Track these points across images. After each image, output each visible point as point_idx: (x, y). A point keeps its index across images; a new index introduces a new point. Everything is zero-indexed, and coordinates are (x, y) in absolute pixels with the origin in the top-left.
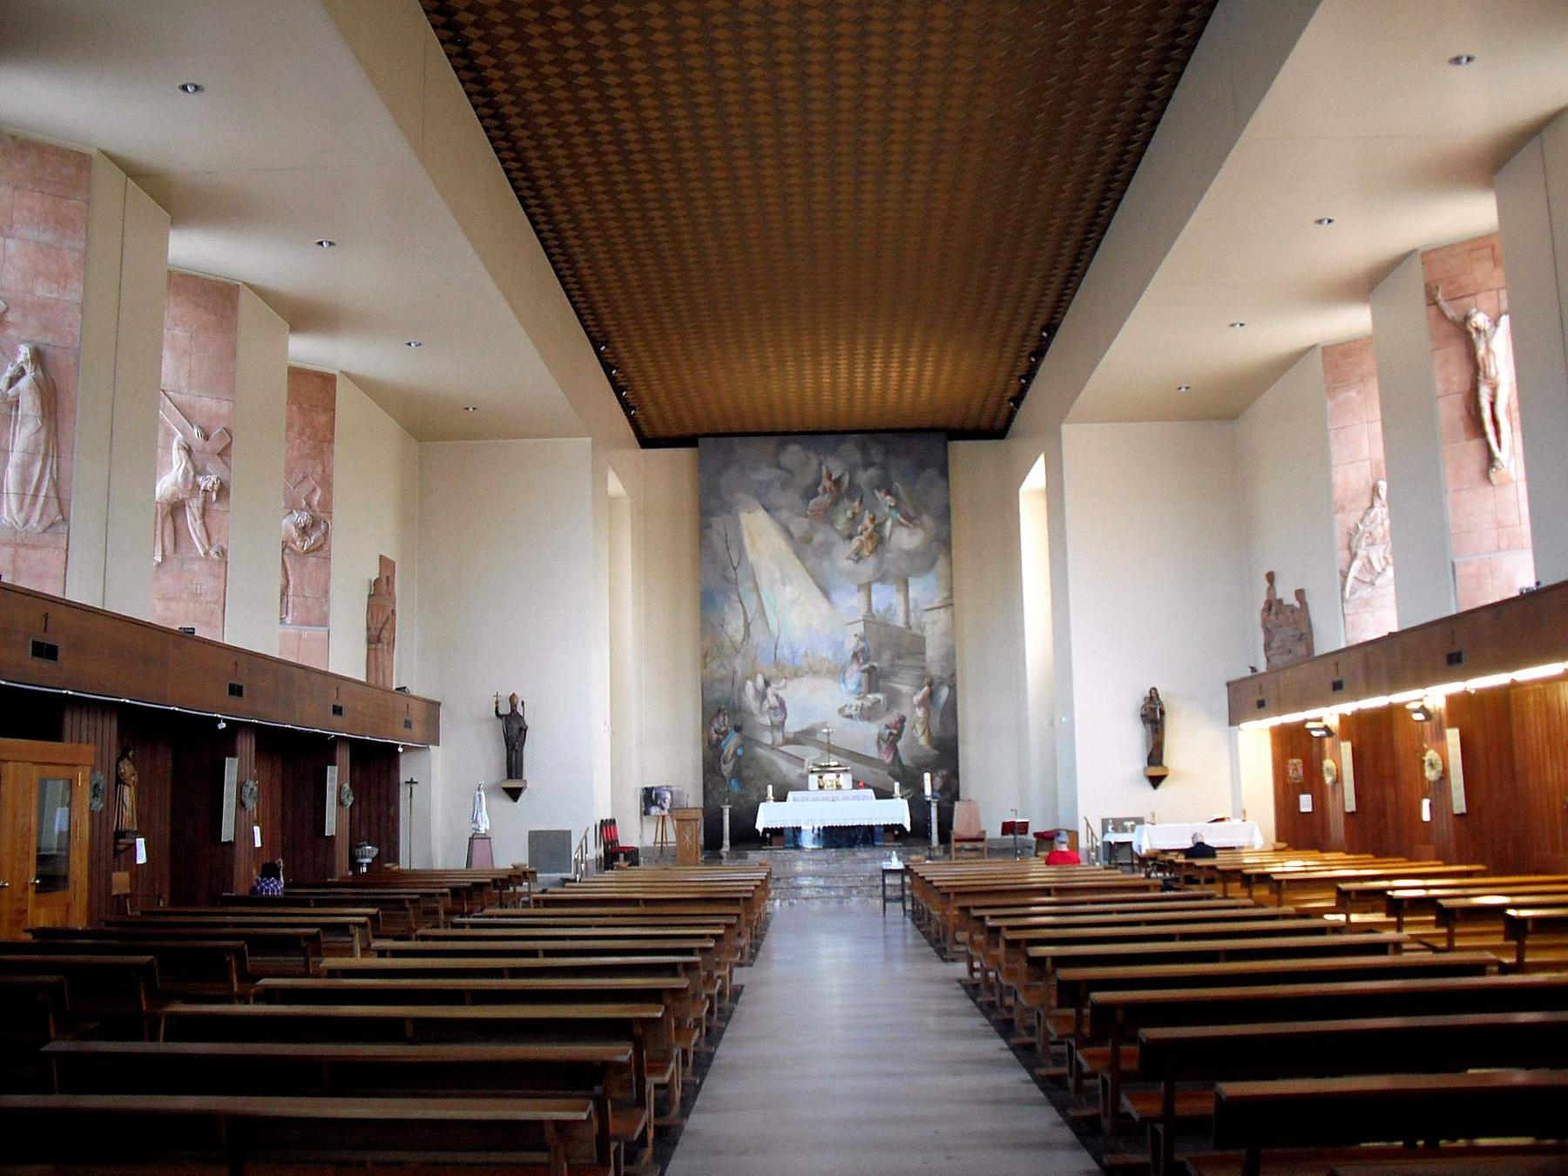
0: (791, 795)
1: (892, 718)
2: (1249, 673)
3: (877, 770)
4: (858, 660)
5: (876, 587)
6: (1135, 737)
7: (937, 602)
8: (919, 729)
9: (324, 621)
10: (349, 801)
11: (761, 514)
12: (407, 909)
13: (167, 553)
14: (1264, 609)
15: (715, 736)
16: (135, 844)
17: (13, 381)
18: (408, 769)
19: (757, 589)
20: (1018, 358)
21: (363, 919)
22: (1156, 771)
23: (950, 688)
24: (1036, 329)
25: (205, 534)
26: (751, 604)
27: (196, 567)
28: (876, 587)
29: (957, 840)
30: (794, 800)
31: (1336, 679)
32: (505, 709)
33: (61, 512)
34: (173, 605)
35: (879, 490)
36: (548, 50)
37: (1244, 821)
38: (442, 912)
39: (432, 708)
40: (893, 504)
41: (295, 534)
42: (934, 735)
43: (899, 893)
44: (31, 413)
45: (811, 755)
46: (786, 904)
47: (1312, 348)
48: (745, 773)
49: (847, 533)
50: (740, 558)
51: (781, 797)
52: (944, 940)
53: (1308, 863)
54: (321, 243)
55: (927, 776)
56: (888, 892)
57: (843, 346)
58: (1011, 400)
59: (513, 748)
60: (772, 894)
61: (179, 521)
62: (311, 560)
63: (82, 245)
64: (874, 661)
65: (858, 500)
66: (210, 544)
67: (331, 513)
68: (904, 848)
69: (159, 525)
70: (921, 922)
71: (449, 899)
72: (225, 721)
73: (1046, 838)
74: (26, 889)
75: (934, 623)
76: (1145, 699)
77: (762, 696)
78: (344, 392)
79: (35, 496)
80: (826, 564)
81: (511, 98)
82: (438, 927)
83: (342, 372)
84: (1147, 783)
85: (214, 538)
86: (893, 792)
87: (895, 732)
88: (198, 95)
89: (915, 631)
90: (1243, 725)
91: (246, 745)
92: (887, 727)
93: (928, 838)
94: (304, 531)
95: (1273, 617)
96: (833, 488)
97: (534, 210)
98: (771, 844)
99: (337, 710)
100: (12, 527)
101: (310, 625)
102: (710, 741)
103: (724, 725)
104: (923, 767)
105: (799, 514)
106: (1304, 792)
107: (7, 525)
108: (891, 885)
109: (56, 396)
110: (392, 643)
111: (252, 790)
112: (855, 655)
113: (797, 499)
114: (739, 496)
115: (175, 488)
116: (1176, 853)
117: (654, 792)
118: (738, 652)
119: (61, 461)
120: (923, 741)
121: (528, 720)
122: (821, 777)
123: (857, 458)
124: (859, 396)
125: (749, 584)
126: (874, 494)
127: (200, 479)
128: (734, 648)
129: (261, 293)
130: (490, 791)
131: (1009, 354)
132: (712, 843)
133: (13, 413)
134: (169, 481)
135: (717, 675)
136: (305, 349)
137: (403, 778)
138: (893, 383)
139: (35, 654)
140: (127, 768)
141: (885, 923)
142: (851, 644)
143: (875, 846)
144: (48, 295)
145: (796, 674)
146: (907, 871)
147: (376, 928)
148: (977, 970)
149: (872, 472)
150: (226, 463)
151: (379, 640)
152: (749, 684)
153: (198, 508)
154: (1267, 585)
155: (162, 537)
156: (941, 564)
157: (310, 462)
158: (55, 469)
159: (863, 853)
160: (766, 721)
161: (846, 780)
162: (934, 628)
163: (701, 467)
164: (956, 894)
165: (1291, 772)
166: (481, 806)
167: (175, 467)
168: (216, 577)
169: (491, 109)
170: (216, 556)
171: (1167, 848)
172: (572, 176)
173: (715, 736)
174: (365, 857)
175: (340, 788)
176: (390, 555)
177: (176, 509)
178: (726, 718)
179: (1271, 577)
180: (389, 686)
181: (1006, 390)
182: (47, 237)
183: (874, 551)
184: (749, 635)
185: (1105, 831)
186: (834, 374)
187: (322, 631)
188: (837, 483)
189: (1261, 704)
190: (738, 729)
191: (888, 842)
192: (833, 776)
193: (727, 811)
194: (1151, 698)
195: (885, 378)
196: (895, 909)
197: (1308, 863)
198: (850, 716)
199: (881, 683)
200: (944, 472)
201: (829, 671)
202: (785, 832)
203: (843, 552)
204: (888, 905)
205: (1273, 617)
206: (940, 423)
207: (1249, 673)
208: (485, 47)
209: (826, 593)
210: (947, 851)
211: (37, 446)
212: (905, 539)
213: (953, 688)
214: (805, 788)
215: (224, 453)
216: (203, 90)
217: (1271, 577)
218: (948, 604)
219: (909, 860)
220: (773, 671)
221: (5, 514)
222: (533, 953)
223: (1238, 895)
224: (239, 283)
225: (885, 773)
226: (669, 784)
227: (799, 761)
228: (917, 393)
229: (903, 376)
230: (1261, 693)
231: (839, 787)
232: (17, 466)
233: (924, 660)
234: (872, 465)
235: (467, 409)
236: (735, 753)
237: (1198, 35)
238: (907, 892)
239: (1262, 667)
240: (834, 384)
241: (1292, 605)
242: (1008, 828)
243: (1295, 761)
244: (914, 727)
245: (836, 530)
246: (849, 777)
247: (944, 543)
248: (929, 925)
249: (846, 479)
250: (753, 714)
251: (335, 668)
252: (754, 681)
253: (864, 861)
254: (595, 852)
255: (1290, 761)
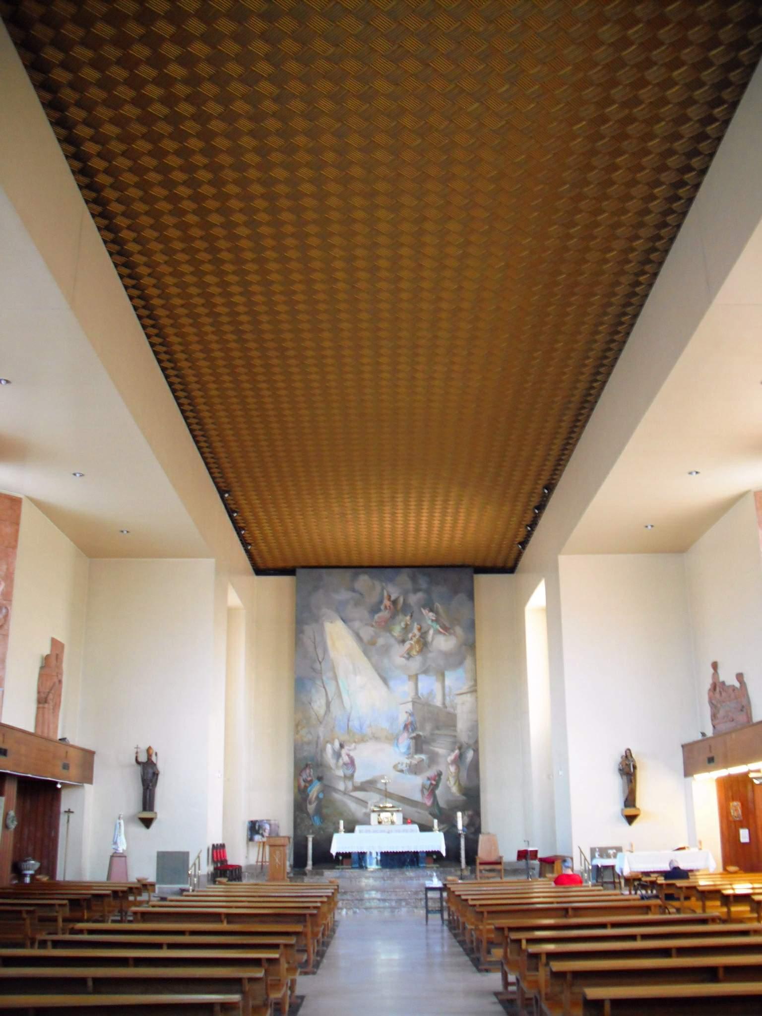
0: (358, 828)
1: (431, 773)
2: (700, 737)
3: (419, 810)
4: (408, 730)
5: (421, 677)
6: (615, 785)
7: (465, 688)
8: (452, 781)
11: (340, 624)
12: (24, 919)
14: (710, 690)
15: (303, 784)
18: (67, 801)
19: (335, 678)
20: (525, 512)
22: (630, 811)
23: (474, 750)
24: (540, 487)
26: (331, 688)
28: (421, 677)
29: (481, 864)
30: (360, 832)
31: (710, 755)
32: (143, 758)
35: (424, 609)
36: (217, 342)
37: (700, 849)
38: (60, 920)
39: (88, 756)
40: (434, 618)
42: (463, 784)
43: (438, 905)
45: (373, 798)
46: (350, 913)
47: (739, 498)
48: (325, 811)
49: (400, 638)
50: (324, 654)
51: (350, 829)
52: (478, 950)
53: (756, 885)
55: (459, 814)
56: (430, 904)
57: (400, 498)
58: (520, 543)
59: (148, 788)
60: (340, 904)
64: (420, 731)
65: (410, 615)
68: (442, 869)
70: (456, 931)
71: (67, 909)
73: (549, 862)
75: (463, 704)
76: (622, 757)
77: (338, 755)
80: (386, 661)
81: (198, 386)
82: (56, 933)
83: (28, 497)
84: (624, 822)
86: (433, 827)
87: (434, 782)
89: (450, 709)
90: (696, 776)
92: (429, 779)
93: (459, 861)
95: (717, 695)
96: (392, 606)
98: (342, 864)
102: (299, 786)
103: (310, 775)
104: (455, 809)
105: (367, 624)
106: (742, 827)
108: (432, 899)
110: (57, 706)
112: (406, 727)
113: (366, 614)
114: (324, 610)
116: (656, 875)
117: (257, 824)
118: (321, 723)
120: (454, 789)
121: (160, 766)
122: (379, 815)
123: (409, 585)
124: (411, 539)
125: (330, 674)
126: (421, 611)
128: (318, 720)
129: (39, 504)
130: (129, 820)
131: (519, 508)
132: (299, 861)
135: (305, 739)
137: (64, 807)
138: (436, 530)
141: (427, 931)
142: (403, 718)
143: (419, 867)
145: (363, 740)
146: (444, 888)
148: (512, 984)
149: (420, 595)
151: (46, 701)
152: (329, 746)
154: (712, 671)
156: (468, 662)
159: (410, 873)
160: (340, 773)
161: (398, 818)
162: (463, 707)
163: (298, 590)
164: (489, 912)
165: (732, 811)
166: (120, 832)
171: (649, 870)
172: (233, 435)
173: (303, 784)
174: (29, 869)
178: (312, 770)
179: (715, 666)
180: (51, 736)
181: (515, 536)
183: (421, 651)
184: (329, 711)
185: (593, 857)
186: (393, 521)
188: (395, 602)
189: (711, 760)
190: (320, 779)
191: (429, 864)
192: (388, 814)
193: (310, 839)
194: (626, 757)
195: (430, 525)
196: (435, 919)
197: (756, 885)
198: (402, 771)
199: (425, 747)
200: (471, 596)
201: (387, 738)
202: (353, 856)
203: (398, 654)
204: (430, 916)
205: (717, 695)
206: (468, 561)
207: (700, 737)
208: (153, 281)
209: (385, 681)
210: (473, 871)
212: (443, 643)
213: (476, 751)
214: (367, 822)
217: (715, 666)
218: (474, 690)
219: (446, 880)
220: (344, 737)
222: (159, 946)
223: (715, 909)
225: (427, 813)
226: (269, 818)
227: (364, 803)
228: (452, 538)
229: (443, 522)
230: (711, 751)
231: (393, 823)
233: (455, 731)
234: (418, 590)
236: (317, 797)
237: (616, 359)
238: (444, 904)
239: (709, 732)
240: (393, 530)
241: (734, 686)
242: (523, 855)
243: (735, 803)
244: (448, 779)
245: (393, 636)
246: (400, 815)
247: (470, 646)
248: (464, 934)
249: (401, 600)
250: (331, 768)
252: (332, 744)
253: (411, 878)
254: (206, 868)
255: (731, 804)
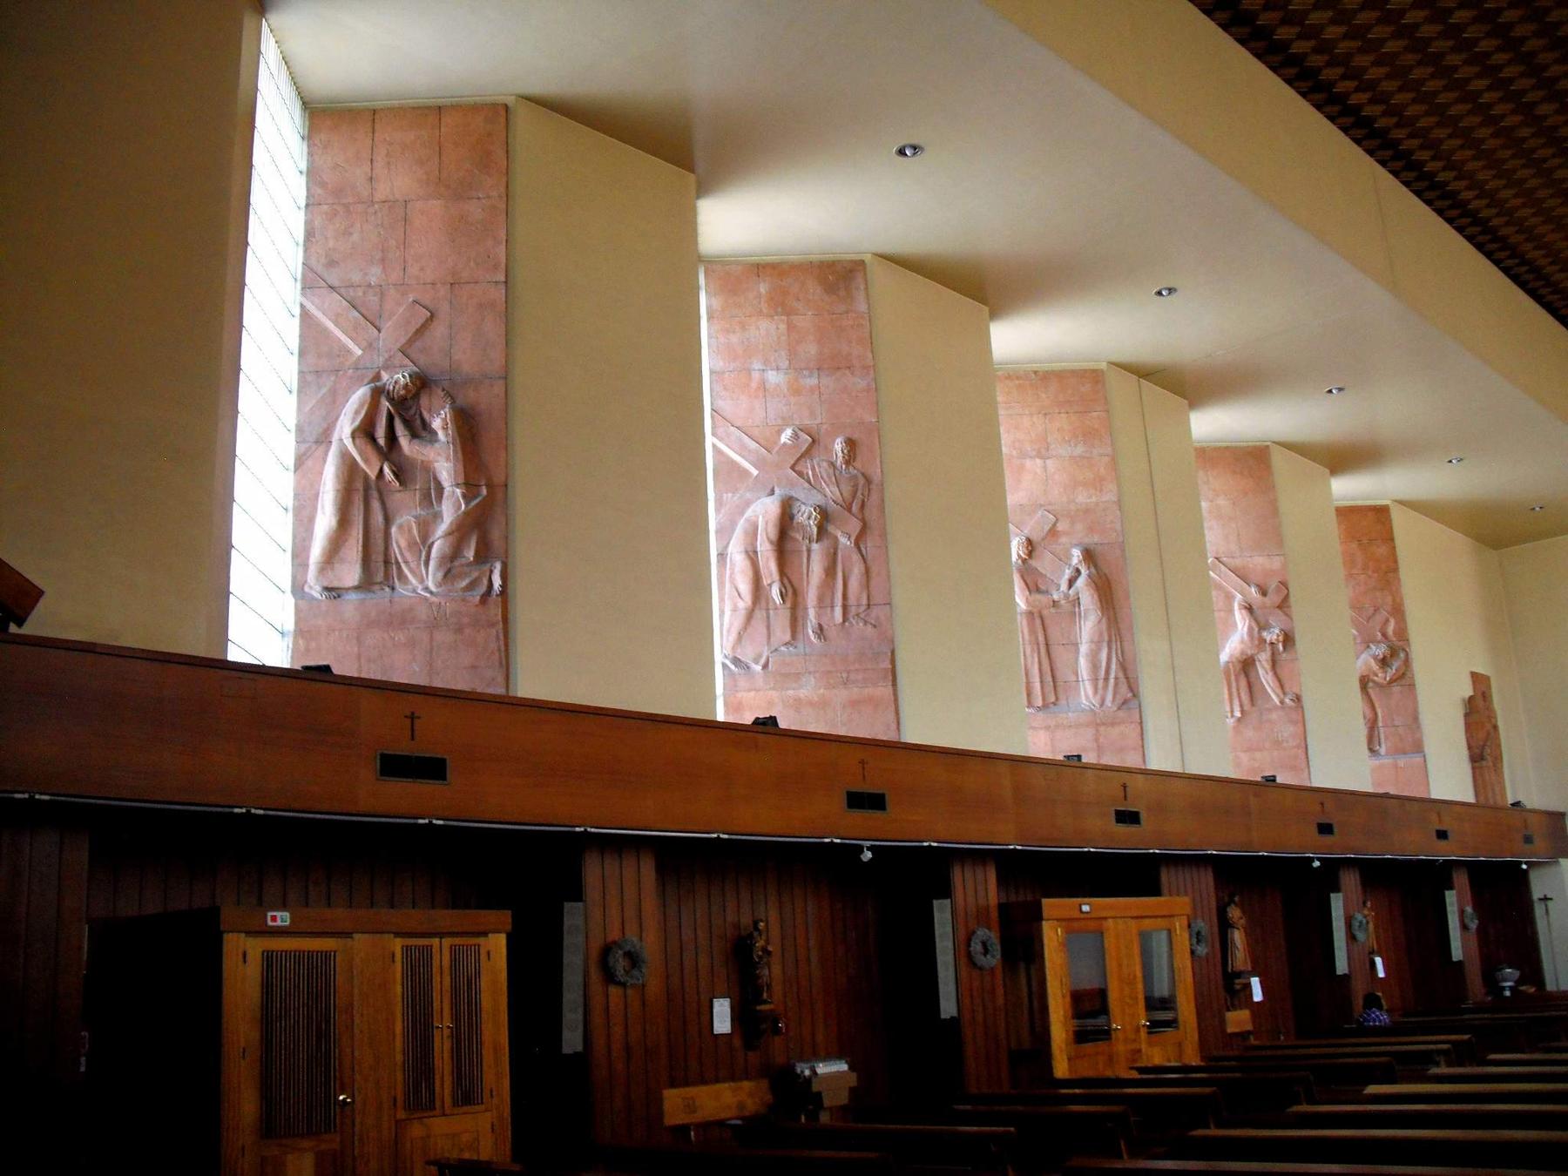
9: (1418, 748)
10: (1473, 925)
13: (1245, 708)
16: (1250, 983)
17: (1071, 583)
21: (1445, 1046)
25: (1277, 684)
27: (1274, 716)
33: (1131, 689)
34: (1258, 755)
41: (1375, 667)
44: (1091, 607)
54: (1330, 391)
61: (1252, 675)
62: (1396, 689)
63: (1109, 450)
66: (1284, 693)
67: (1408, 640)
69: (1234, 685)
72: (1318, 859)
74: (1137, 1030)
78: (1398, 518)
79: (1106, 679)
85: (1287, 690)
88: (1174, 296)
91: (1350, 880)
94: (1384, 662)
97: (1550, 298)
99: (1442, 835)
100: (1092, 710)
101: (1405, 753)
107: (1087, 708)
109: (1110, 588)
111: (1361, 922)
115: (1243, 646)
119: (1125, 644)
127: (1265, 634)
133: (1077, 609)
134: (1234, 644)
136: (1348, 488)
137: (1537, 894)
139: (1118, 821)
140: (1234, 913)
144: (1088, 501)
147: (1458, 1055)
150: (1287, 615)
153: (1267, 660)
155: (1239, 694)
157: (1378, 594)
158: (1119, 652)
167: (1240, 626)
168: (1294, 723)
169: (1468, 217)
170: (1291, 703)
175: (1462, 912)
176: (1480, 670)
177: (1246, 665)
180: (1500, 803)
182: (1080, 450)
187: (1418, 759)
211: (1101, 634)
215: (1284, 605)
216: (1175, 290)
221: (1083, 698)
224: (1269, 443)
232: (1087, 655)
235: (1534, 509)
251: (1438, 792)
